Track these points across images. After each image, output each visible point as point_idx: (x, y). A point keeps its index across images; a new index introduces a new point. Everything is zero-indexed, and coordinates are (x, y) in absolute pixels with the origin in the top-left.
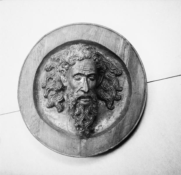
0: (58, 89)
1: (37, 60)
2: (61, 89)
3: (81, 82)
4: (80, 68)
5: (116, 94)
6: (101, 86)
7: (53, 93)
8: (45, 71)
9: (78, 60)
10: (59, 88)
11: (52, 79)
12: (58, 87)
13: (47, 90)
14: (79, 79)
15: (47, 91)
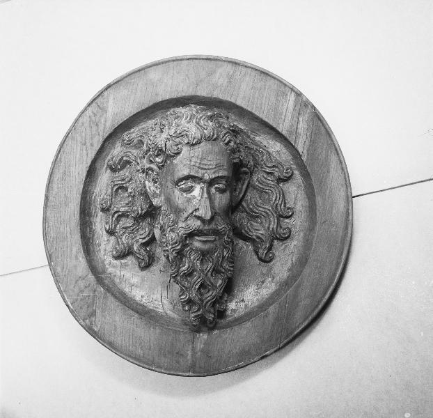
0: (140, 212)
1: (88, 144)
2: (145, 213)
3: (194, 198)
4: (192, 163)
5: (279, 225)
6: (243, 207)
7: (128, 222)
8: (109, 171)
9: (188, 143)
10: (142, 210)
11: (124, 189)
12: (140, 209)
13: (113, 216)
14: (190, 190)
15: (114, 219)
